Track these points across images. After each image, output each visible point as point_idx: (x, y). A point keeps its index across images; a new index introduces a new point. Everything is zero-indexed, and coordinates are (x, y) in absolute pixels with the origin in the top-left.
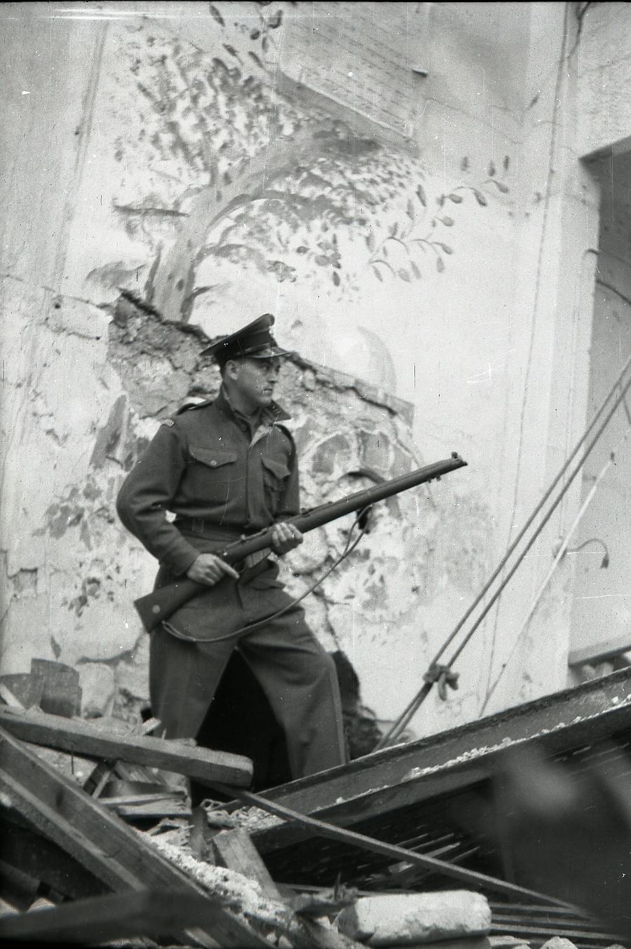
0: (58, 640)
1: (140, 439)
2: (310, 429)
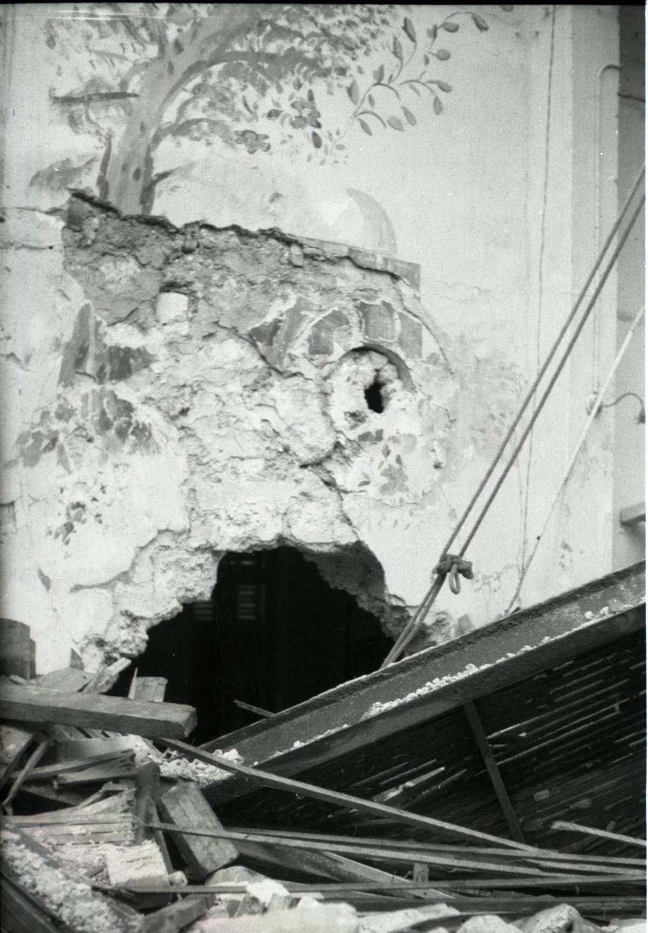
1: (111, 348)
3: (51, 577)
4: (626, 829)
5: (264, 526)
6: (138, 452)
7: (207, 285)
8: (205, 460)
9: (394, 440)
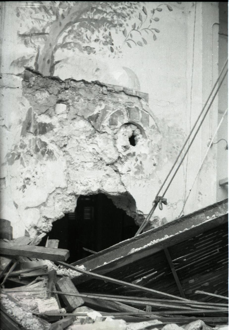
1: (39, 123)
3: (18, 204)
5: (93, 186)
6: (49, 160)
7: (73, 101)
8: (72, 163)
9: (139, 155)
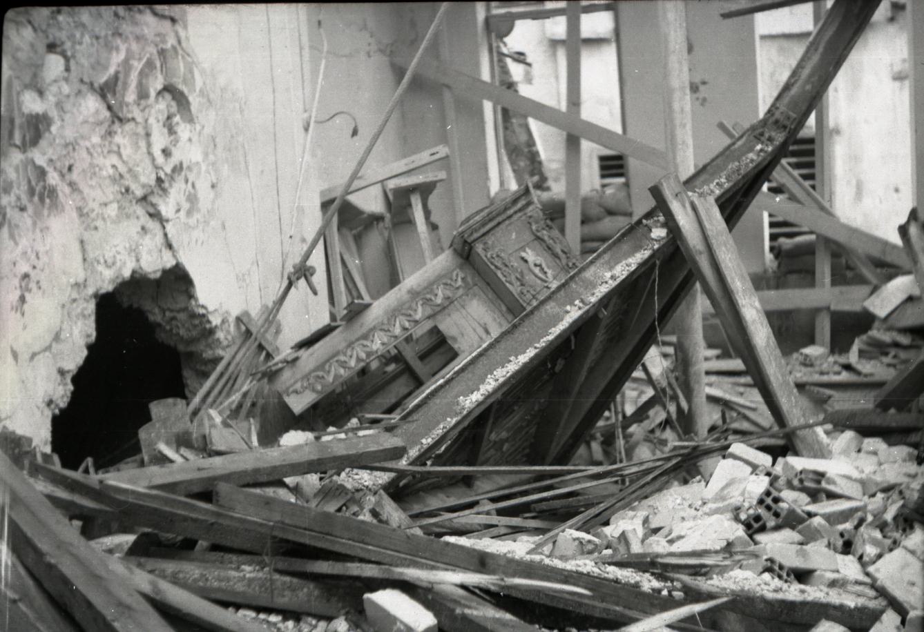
0: (15, 348)
1: (28, 115)
2: (134, 59)
3: (18, 350)
4: (380, 411)
5: (125, 263)
6: (52, 214)
7: (74, 43)
8: (85, 211)
9: (189, 168)
